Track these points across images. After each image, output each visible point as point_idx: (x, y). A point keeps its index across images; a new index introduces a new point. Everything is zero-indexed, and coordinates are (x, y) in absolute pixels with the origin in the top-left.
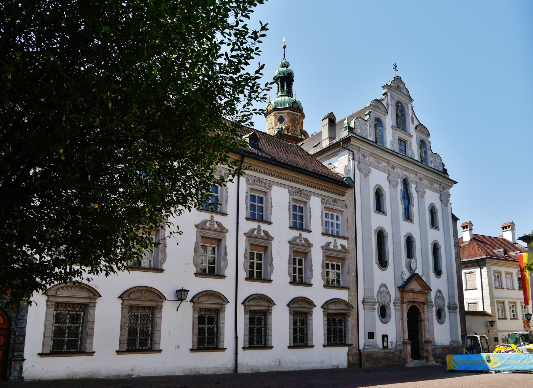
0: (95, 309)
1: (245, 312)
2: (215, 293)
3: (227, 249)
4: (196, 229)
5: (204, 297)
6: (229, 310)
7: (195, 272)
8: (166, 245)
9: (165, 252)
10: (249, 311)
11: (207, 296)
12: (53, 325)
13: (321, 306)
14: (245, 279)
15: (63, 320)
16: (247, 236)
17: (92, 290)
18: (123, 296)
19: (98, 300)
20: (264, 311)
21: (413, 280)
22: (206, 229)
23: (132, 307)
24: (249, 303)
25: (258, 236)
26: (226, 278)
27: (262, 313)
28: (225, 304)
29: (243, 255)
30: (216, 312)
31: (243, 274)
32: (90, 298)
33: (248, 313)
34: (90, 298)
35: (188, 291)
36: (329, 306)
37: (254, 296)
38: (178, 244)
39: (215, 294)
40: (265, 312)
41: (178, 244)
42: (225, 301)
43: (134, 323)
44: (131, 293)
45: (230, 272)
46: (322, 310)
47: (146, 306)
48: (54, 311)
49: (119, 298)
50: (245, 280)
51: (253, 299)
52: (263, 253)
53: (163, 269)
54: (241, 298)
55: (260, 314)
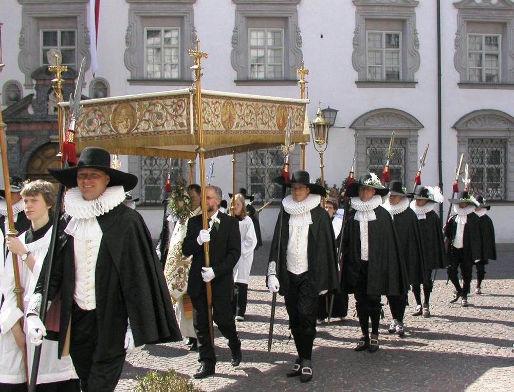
0: (417, 145)
1: (459, 142)
2: (385, 111)
3: (419, 36)
4: (355, 7)
5: (376, 119)
6: (426, 140)
7: (459, 82)
8: (417, 43)
9: (417, 55)
10: (466, 140)
11: (381, 118)
12: (367, 168)
13: (452, 126)
14: (459, 84)
15: (380, 160)
16: (459, 9)
17: (411, 118)
18: (458, 126)
19: (420, 133)
20: (501, 140)
21: (249, 51)
22: (375, 6)
23: (473, 140)
24: (467, 126)
25: (486, 4)
26: (416, 85)
27: (497, 143)
28: (417, 130)
29: (453, 42)
30: (401, 143)
31: (451, 76)
32: (410, 130)
33: (467, 144)
34: (509, 130)
35: (336, 111)
36: (366, 124)
37: (476, 114)
38: (322, 37)
39: (396, 114)
40: (503, 141)
41: (322, 37)
42: (417, 125)
43: (257, 164)
44: (368, 119)
45: (425, 74)
46: (455, 133)
47: (475, 138)
48: (469, 147)
49: (452, 128)
50: (458, 87)
51: (474, 119)
52: (500, 35)
53: (415, 81)
54: (449, 119)
55: (492, 145)
